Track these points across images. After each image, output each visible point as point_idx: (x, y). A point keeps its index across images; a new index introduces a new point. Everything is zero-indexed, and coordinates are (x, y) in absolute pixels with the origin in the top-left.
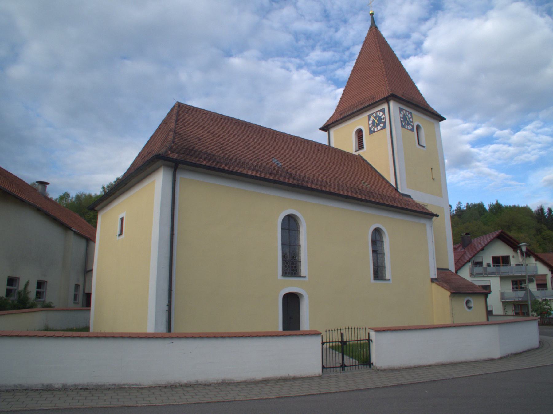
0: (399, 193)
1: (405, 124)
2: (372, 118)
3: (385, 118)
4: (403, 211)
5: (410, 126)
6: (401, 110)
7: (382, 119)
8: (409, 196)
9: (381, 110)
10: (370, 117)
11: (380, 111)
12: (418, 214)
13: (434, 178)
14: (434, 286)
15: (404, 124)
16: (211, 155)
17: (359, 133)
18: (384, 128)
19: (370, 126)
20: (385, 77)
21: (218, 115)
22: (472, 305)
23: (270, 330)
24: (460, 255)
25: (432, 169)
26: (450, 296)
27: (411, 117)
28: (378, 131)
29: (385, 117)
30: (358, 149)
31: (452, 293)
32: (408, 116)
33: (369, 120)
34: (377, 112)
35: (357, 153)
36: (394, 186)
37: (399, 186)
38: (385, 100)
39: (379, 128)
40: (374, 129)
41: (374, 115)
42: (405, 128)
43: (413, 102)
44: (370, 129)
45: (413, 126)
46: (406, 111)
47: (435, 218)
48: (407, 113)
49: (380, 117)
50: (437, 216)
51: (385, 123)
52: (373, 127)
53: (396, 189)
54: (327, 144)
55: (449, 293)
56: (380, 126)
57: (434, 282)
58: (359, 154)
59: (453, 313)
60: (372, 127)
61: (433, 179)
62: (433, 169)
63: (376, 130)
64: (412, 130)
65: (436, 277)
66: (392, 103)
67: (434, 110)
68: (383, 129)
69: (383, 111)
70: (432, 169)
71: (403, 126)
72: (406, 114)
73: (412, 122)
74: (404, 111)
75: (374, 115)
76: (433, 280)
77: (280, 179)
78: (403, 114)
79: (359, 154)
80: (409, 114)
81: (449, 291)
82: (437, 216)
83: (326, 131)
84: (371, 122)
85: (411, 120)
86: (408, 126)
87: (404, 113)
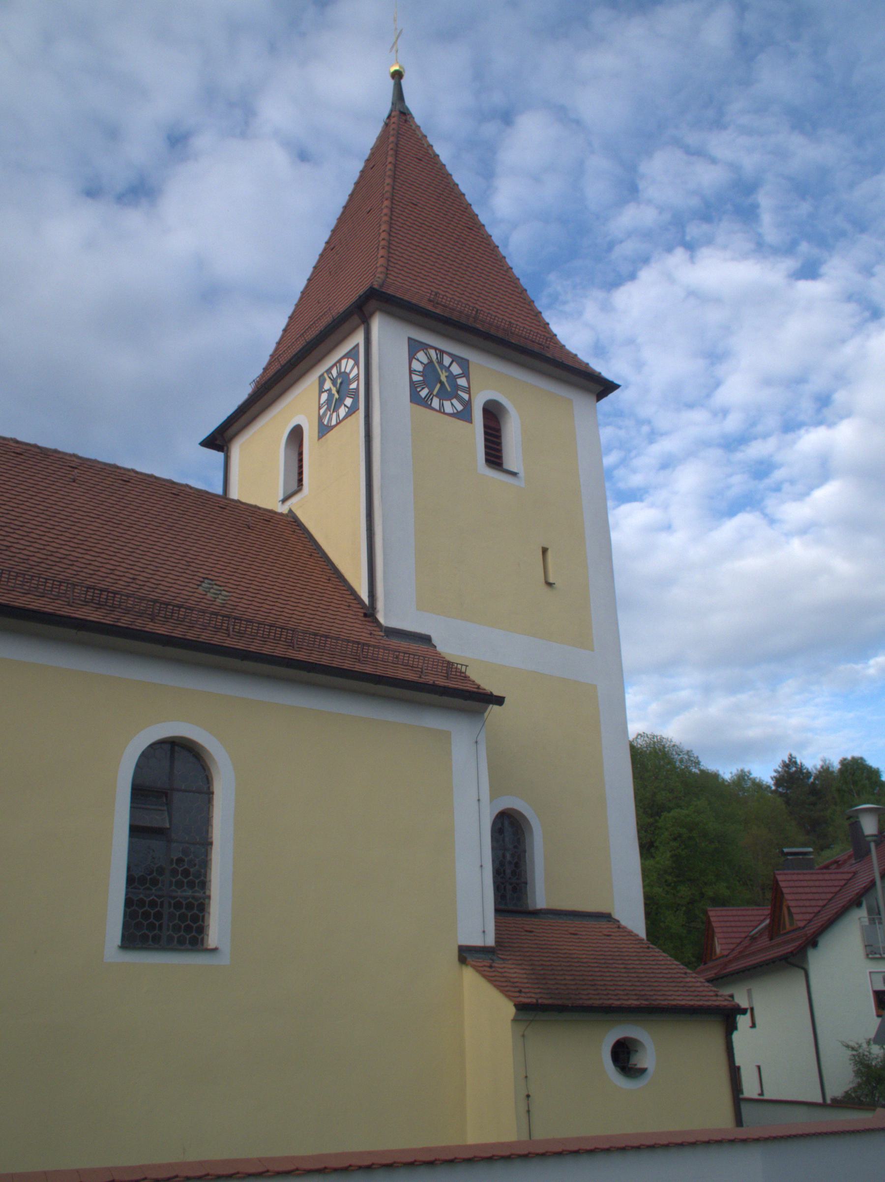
0: (376, 621)
1: (431, 392)
2: (328, 385)
3: (357, 377)
4: (381, 689)
5: (343, 370)
6: (414, 347)
7: (350, 382)
8: (426, 639)
9: (347, 354)
10: (325, 380)
11: (347, 356)
12: (397, 692)
13: (551, 580)
14: (469, 976)
15: (424, 393)
16: (234, 618)
17: (296, 434)
18: (352, 411)
19: (322, 411)
20: (380, 248)
21: (139, 476)
22: (647, 1059)
23: (218, 1157)
24: (823, 896)
25: (545, 551)
26: (515, 1020)
27: (466, 374)
28: (441, 411)
29: (444, 413)
30: (220, 455)
31: (521, 1008)
32: (448, 369)
33: (321, 391)
34: (339, 361)
35: (283, 509)
36: (365, 596)
37: (380, 605)
38: (356, 319)
39: (342, 411)
40: (330, 419)
41: (334, 372)
42: (430, 407)
43: (478, 326)
44: (320, 418)
45: (468, 405)
46: (442, 352)
47: (494, 709)
48: (447, 360)
49: (344, 375)
50: (499, 701)
51: (355, 394)
52: (329, 413)
53: (370, 613)
54: (219, 491)
55: (509, 1009)
56: (345, 406)
57: (469, 960)
58: (290, 511)
59: (528, 1096)
60: (325, 413)
61: (549, 584)
62: (550, 554)
63: (334, 422)
64: (465, 415)
65: (490, 941)
66: (378, 324)
67: (579, 359)
68: (350, 415)
69: (352, 354)
70: (545, 551)
71: (415, 398)
72: (440, 362)
73: (468, 390)
74: (432, 352)
75: (334, 372)
76: (466, 954)
77: (125, 621)
78: (425, 360)
79: (290, 511)
80: (454, 364)
81: (509, 997)
82: (499, 701)
83: (219, 448)
84: (324, 396)
85: (462, 382)
86: (348, 371)
87: (430, 358)
